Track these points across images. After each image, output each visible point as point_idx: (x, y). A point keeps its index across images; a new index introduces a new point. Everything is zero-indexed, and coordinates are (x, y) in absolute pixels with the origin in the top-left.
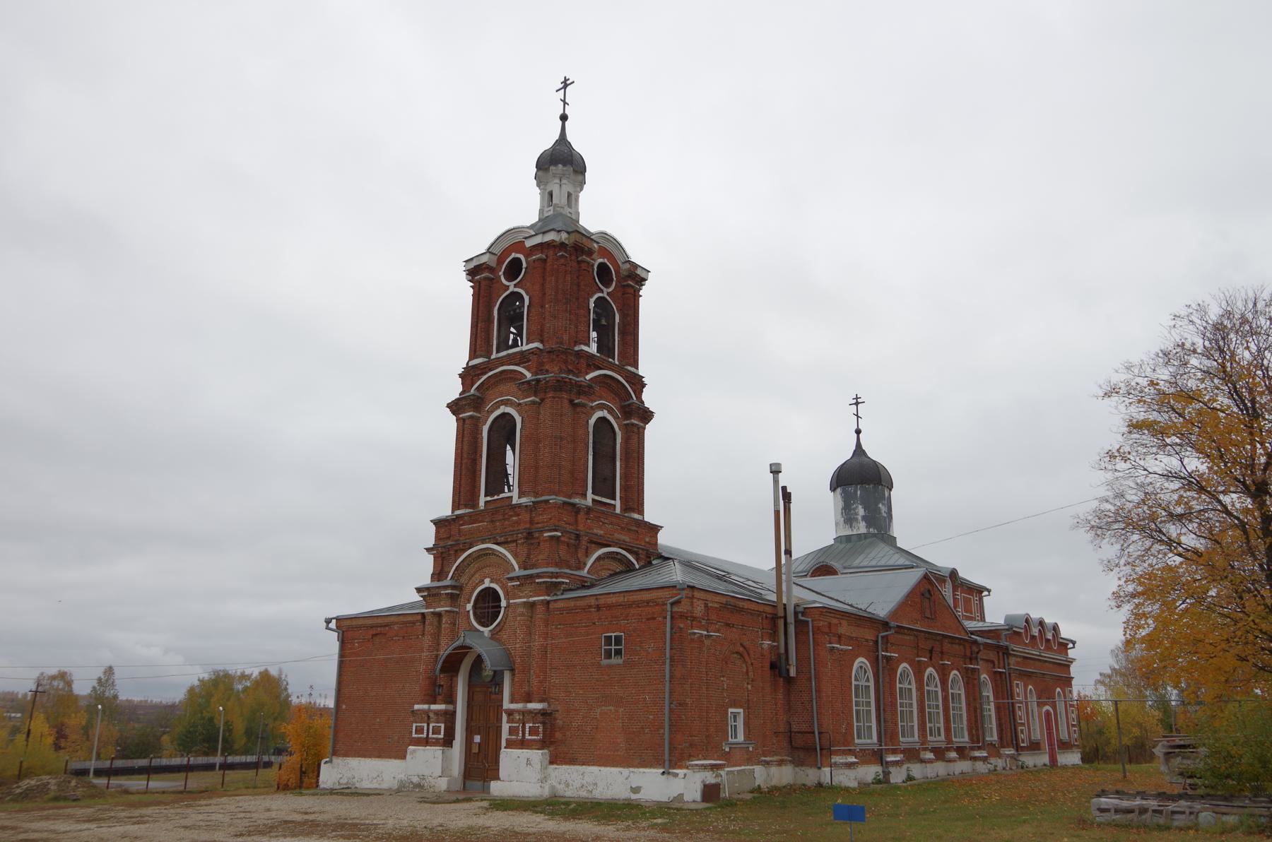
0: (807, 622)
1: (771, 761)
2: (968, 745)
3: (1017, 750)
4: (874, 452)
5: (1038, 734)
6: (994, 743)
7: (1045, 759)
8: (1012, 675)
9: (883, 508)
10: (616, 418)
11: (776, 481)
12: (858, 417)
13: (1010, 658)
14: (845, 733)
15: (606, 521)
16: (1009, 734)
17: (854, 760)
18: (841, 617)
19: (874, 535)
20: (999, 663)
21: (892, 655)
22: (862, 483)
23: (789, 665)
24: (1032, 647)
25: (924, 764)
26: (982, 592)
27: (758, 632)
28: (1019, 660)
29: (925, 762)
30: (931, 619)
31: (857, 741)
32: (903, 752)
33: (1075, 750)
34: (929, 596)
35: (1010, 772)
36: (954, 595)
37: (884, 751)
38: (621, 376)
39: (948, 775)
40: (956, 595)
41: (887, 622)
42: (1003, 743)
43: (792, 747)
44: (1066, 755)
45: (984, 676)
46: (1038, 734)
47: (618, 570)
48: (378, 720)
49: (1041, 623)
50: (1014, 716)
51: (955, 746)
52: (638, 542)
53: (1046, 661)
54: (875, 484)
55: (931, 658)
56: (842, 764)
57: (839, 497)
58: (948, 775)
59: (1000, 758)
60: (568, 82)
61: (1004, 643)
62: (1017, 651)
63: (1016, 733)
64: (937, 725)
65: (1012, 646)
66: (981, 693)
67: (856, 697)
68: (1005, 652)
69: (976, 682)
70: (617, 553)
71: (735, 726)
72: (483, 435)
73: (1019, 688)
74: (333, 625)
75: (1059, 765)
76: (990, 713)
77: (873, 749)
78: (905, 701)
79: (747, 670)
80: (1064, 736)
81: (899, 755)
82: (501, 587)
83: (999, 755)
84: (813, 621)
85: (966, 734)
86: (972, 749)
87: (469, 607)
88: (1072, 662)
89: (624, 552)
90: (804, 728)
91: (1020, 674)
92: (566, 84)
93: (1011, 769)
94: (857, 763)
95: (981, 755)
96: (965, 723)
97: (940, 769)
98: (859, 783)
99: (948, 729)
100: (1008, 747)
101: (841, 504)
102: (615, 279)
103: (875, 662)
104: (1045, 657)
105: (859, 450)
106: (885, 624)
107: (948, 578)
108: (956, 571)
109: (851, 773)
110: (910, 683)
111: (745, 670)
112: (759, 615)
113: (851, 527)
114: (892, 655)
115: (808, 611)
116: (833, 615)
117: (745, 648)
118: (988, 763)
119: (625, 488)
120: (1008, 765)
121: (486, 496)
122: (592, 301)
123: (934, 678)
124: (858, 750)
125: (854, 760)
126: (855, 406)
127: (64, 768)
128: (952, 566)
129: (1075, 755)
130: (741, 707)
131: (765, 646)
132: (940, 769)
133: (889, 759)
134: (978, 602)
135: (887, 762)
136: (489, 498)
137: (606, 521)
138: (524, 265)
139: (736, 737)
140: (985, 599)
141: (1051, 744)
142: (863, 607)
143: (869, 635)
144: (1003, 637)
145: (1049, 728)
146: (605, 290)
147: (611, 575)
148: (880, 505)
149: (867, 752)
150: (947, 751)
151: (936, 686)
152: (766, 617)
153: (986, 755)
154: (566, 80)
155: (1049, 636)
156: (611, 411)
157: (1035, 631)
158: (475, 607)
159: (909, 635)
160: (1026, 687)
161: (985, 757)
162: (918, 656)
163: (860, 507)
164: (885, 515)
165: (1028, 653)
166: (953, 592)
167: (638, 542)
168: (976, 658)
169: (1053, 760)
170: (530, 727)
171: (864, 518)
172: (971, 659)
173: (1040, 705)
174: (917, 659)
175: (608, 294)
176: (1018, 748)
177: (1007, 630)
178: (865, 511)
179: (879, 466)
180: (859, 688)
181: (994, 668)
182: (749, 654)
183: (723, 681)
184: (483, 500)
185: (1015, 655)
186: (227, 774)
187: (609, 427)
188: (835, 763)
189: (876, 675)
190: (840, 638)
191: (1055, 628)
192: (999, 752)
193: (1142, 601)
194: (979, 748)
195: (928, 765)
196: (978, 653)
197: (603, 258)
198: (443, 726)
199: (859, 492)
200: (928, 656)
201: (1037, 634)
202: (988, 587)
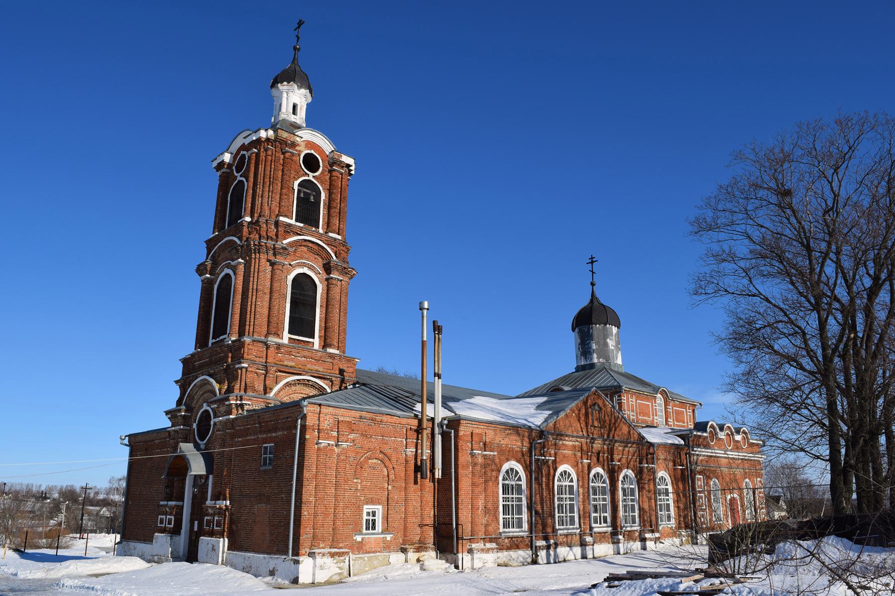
10: (317, 273)
12: (593, 272)
15: (298, 355)
27: (402, 441)
38: (321, 240)
47: (311, 394)
52: (332, 371)
60: (594, 260)
70: (308, 381)
74: (126, 441)
76: (668, 502)
92: (300, 23)
101: (579, 340)
113: (585, 358)
117: (385, 454)
118: (661, 542)
122: (296, 183)
130: (379, 504)
136: (214, 341)
137: (298, 355)
139: (375, 529)
146: (311, 174)
154: (300, 21)
164: (613, 348)
166: (665, 406)
167: (332, 371)
183: (356, 483)
184: (211, 341)
186: (81, 550)
198: (159, 517)
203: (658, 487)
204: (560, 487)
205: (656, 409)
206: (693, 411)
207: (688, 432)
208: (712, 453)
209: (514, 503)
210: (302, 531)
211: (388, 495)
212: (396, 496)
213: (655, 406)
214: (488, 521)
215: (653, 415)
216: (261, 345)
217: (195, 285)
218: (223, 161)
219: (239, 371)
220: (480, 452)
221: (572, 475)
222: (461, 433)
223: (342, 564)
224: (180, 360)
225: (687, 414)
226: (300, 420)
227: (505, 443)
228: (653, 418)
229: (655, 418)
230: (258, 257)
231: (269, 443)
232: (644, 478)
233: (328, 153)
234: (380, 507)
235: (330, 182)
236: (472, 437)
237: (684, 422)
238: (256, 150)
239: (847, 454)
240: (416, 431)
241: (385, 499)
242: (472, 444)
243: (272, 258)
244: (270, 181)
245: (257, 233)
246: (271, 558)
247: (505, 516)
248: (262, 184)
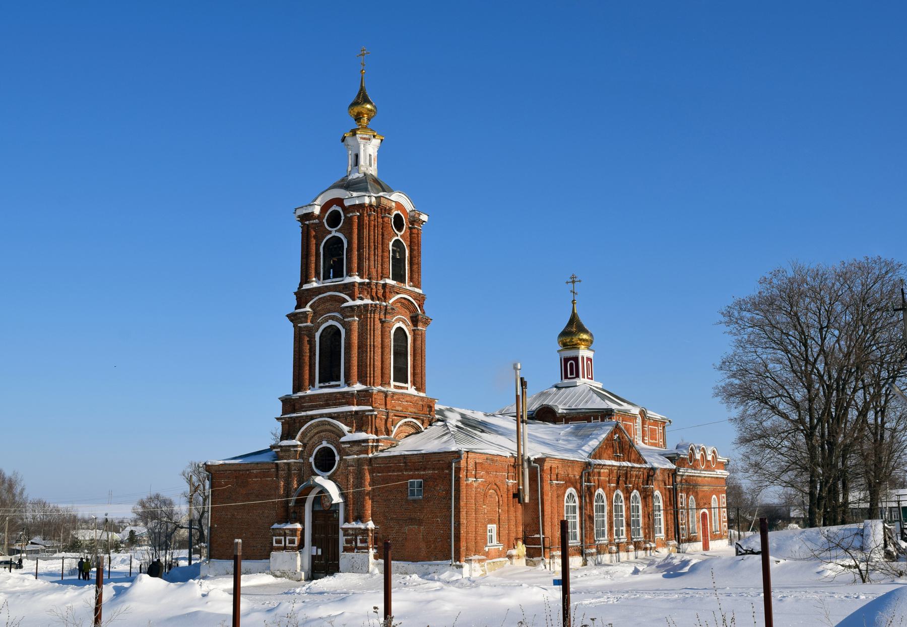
10: (407, 325)
15: (403, 400)
27: (505, 475)
38: (410, 296)
47: (410, 433)
48: (244, 535)
67: (567, 513)
70: (411, 422)
71: (491, 535)
72: (316, 339)
78: (601, 514)
79: (499, 500)
82: (335, 447)
87: (312, 460)
89: (414, 421)
100: (672, 540)
102: (405, 224)
110: (603, 502)
111: (497, 500)
117: (497, 486)
118: (656, 551)
119: (414, 374)
121: (320, 382)
123: (620, 497)
127: (129, 571)
131: (510, 484)
134: (662, 431)
137: (403, 400)
138: (343, 218)
139: (492, 542)
147: (406, 436)
156: (404, 322)
158: (315, 459)
166: (642, 425)
170: (360, 539)
175: (401, 236)
182: (500, 490)
187: (405, 339)
197: (398, 211)
205: (636, 429)
206: (664, 427)
207: (675, 455)
208: (695, 473)
210: (461, 545)
211: (499, 516)
212: (504, 517)
215: (634, 435)
216: (382, 394)
217: (289, 329)
218: (313, 212)
219: (370, 417)
221: (603, 497)
222: (545, 468)
223: (483, 568)
224: (279, 399)
226: (454, 464)
230: (372, 316)
231: (417, 479)
232: (647, 496)
233: (408, 211)
234: (495, 526)
235: (411, 239)
236: (551, 470)
237: (656, 440)
238: (358, 214)
239: (821, 490)
240: (513, 466)
241: (497, 519)
242: (551, 476)
243: (382, 317)
244: (375, 246)
245: (368, 293)
246: (430, 565)
248: (367, 247)
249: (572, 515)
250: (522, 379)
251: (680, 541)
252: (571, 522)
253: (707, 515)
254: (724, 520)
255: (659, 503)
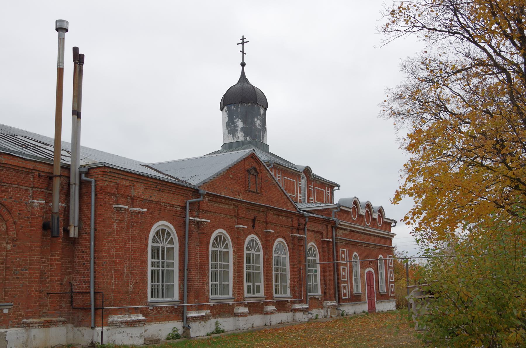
0: (90, 182)
1: (32, 323)
2: (289, 300)
3: (339, 302)
4: (254, 80)
5: (359, 288)
6: (317, 297)
7: (365, 307)
8: (338, 244)
9: (258, 122)
11: (61, 40)
12: (243, 53)
13: (338, 231)
14: (133, 293)
16: (332, 290)
17: (141, 317)
18: (134, 179)
19: (250, 142)
20: (327, 234)
21: (203, 220)
22: (242, 102)
23: (69, 225)
24: (360, 223)
25: (237, 318)
26: (334, 187)
27: (27, 190)
28: (346, 232)
29: (238, 316)
30: (258, 193)
31: (150, 299)
32: (212, 308)
33: (391, 299)
34: (255, 174)
35: (331, 319)
36: (308, 187)
37: (185, 308)
39: (266, 325)
40: (310, 187)
41: (198, 190)
42: (325, 296)
43: (73, 308)
44: (383, 304)
45: (311, 244)
46: (359, 288)
49: (368, 206)
50: (338, 276)
51: (275, 301)
53: (371, 235)
54: (252, 104)
55: (253, 227)
56: (121, 322)
57: (225, 113)
58: (266, 325)
59: (322, 309)
60: (245, 40)
61: (333, 218)
62: (344, 225)
63: (339, 289)
64: (256, 284)
65: (339, 221)
66: (305, 257)
68: (334, 226)
69: (302, 248)
73: (344, 254)
75: (377, 311)
76: (315, 273)
77: (173, 307)
80: (383, 289)
81: (204, 311)
83: (322, 307)
84: (96, 181)
85: (289, 290)
86: (294, 302)
88: (393, 236)
90: (84, 289)
91: (346, 243)
93: (331, 317)
94: (144, 321)
95: (301, 307)
96: (288, 281)
97: (244, 323)
98: (145, 340)
99: (268, 287)
101: (226, 119)
103: (181, 227)
104: (370, 231)
105: (243, 78)
106: (195, 192)
107: (303, 174)
108: (310, 168)
109: (136, 331)
112: (28, 173)
113: (233, 136)
114: (203, 220)
115: (92, 171)
116: (122, 177)
120: (329, 314)
123: (257, 244)
124: (152, 308)
125: (141, 317)
126: (241, 45)
128: (305, 165)
129: (391, 303)
132: (257, 320)
133: (190, 315)
134: (329, 194)
135: (188, 318)
140: (335, 192)
141: (370, 296)
142: (184, 180)
143: (176, 201)
144: (333, 214)
145: (370, 285)
148: (256, 120)
149: (163, 309)
150: (266, 305)
151: (258, 250)
152: (39, 176)
153: (307, 307)
155: (375, 216)
157: (363, 212)
159: (227, 204)
160: (351, 254)
161: (306, 308)
162: (238, 224)
163: (240, 120)
164: (260, 128)
165: (354, 228)
166: (308, 185)
168: (304, 229)
169: (372, 308)
171: (243, 129)
172: (298, 229)
173: (363, 266)
174: (236, 226)
176: (340, 300)
177: (336, 208)
178: (243, 124)
179: (255, 88)
180: (221, 253)
181: (322, 238)
185: (342, 229)
188: (112, 322)
189: (182, 239)
190: (133, 201)
191: (381, 211)
192: (322, 304)
193: (474, 69)
194: (301, 302)
195: (241, 318)
196: (305, 225)
199: (239, 110)
200: (251, 224)
201: (364, 214)
202: (338, 184)
203: (308, 258)
204: (215, 253)
205: (300, 187)
209: (165, 269)
213: (300, 184)
214: (134, 289)
215: (297, 192)
220: (127, 207)
225: (326, 194)
227: (157, 200)
228: (297, 195)
229: (299, 195)
247: (153, 284)
249: (279, 273)
250: (75, 50)
251: (340, 300)
252: (253, 273)
253: (373, 275)
254: (391, 280)
255: (315, 256)
